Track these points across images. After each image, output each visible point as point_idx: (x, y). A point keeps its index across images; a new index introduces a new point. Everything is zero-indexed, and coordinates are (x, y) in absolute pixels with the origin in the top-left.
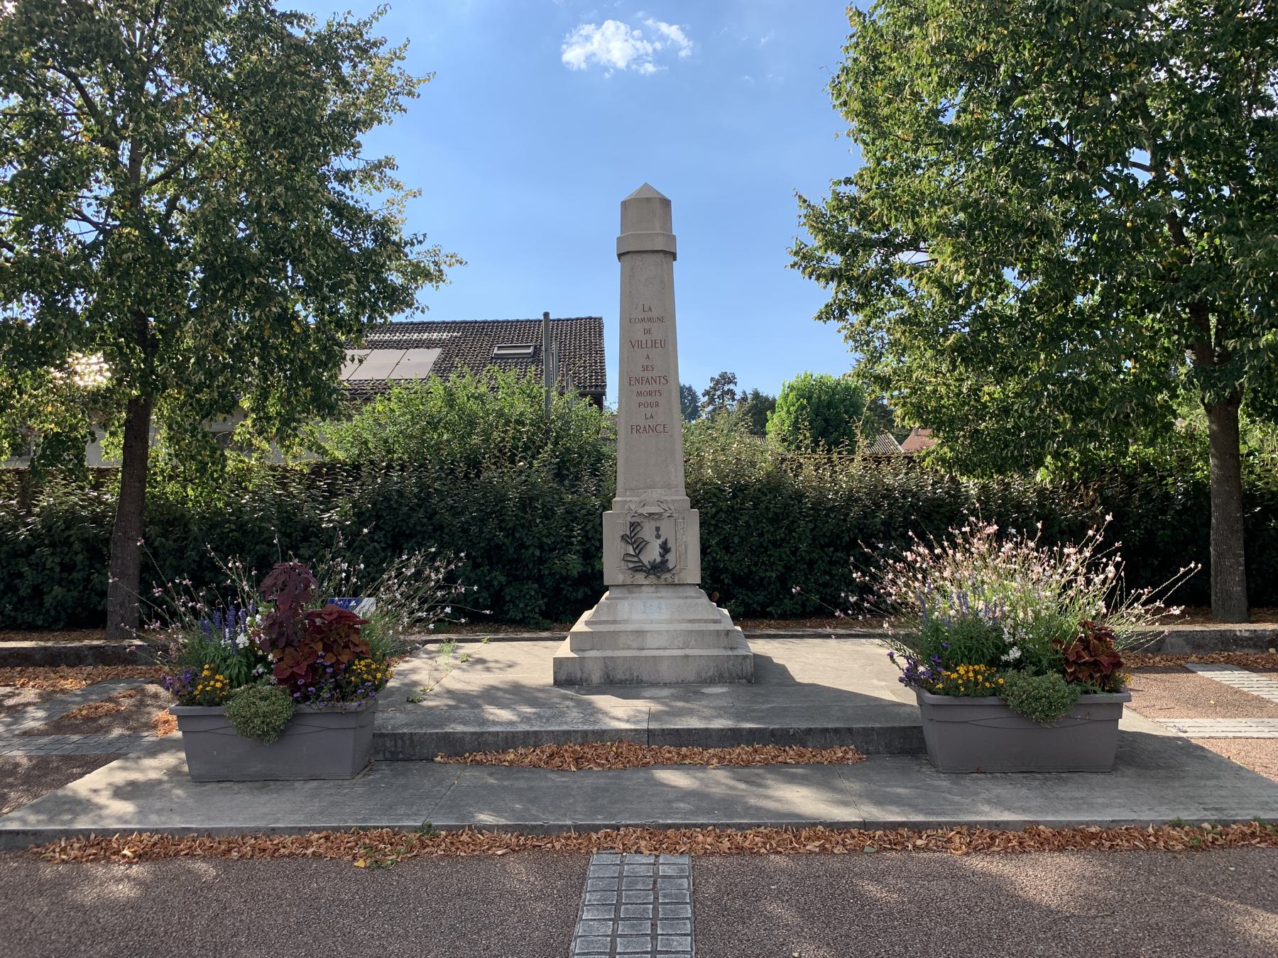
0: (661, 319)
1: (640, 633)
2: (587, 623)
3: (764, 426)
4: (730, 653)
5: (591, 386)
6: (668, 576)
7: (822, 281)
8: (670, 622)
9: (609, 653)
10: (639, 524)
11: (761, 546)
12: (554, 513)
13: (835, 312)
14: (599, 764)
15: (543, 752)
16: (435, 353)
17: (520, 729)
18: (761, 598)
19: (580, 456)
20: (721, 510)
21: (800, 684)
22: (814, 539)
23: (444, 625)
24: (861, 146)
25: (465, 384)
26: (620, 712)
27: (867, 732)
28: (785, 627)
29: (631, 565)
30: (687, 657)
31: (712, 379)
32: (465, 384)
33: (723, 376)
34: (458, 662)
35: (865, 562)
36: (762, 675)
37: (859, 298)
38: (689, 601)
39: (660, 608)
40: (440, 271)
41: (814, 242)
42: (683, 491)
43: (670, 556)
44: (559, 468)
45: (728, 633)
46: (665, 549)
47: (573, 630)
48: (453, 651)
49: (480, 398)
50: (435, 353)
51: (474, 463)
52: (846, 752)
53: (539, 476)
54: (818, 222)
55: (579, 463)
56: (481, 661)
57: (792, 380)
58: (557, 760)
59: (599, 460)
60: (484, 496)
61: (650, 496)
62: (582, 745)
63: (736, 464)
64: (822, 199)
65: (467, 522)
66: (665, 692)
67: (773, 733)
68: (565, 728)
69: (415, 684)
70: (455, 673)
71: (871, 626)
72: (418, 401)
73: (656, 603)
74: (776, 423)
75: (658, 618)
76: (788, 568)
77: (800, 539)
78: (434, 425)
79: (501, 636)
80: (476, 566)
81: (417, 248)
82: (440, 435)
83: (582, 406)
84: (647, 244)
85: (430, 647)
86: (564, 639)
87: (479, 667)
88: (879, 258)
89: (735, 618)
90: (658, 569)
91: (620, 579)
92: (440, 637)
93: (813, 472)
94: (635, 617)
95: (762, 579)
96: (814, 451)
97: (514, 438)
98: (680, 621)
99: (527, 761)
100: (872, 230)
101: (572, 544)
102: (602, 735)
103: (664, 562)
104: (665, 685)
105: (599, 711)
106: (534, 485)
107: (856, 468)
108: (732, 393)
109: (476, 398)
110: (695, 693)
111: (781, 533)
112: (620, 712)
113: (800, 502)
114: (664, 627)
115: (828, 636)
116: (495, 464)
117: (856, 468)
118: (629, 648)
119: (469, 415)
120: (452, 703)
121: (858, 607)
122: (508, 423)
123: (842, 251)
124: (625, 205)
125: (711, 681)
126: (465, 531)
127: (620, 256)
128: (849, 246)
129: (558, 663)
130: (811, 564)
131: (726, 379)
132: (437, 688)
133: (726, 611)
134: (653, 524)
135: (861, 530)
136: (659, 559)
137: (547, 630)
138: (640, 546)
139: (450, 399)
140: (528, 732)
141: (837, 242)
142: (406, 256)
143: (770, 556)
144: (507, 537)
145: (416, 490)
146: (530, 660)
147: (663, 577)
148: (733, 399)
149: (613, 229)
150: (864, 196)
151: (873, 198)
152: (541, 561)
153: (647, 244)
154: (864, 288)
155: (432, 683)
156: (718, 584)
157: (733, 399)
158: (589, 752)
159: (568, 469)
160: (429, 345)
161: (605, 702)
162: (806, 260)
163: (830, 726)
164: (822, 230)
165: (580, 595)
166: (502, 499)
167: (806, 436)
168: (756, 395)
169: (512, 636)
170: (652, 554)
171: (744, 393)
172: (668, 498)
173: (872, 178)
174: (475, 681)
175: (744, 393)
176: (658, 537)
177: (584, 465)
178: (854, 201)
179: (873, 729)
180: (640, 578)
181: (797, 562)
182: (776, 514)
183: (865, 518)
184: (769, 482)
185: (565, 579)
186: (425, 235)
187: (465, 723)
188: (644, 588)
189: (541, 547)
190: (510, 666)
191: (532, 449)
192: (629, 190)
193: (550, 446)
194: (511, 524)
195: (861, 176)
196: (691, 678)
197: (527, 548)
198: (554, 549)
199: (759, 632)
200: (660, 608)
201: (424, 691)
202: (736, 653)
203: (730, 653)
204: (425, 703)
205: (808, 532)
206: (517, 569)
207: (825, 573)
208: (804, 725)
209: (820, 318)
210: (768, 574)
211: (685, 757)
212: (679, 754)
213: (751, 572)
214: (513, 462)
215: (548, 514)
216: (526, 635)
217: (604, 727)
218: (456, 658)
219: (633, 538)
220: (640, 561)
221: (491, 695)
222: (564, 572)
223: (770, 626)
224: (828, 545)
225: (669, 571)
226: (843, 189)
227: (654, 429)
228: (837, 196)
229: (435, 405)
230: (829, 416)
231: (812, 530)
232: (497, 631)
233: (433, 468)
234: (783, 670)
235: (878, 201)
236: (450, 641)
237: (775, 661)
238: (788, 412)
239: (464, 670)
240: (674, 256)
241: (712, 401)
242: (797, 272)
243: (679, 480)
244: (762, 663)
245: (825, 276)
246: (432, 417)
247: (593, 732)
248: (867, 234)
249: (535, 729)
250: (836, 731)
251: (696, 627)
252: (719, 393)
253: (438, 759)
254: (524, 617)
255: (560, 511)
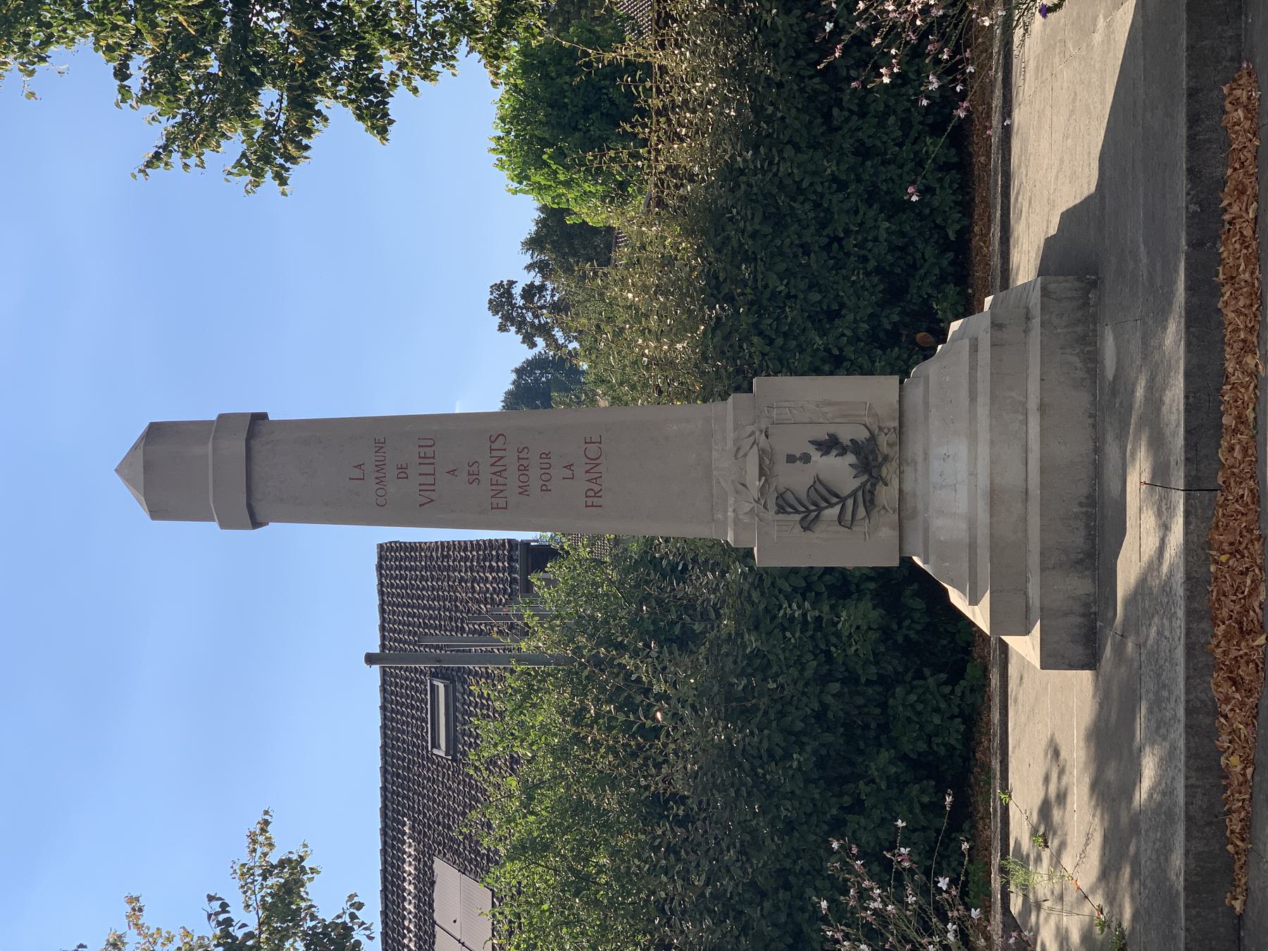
0: (380, 446)
1: (995, 497)
2: (974, 601)
3: (595, 231)
4: (1036, 322)
5: (511, 570)
6: (883, 440)
7: (313, 122)
8: (973, 438)
9: (1034, 560)
10: (781, 496)
11: (827, 248)
12: (757, 653)
13: (373, 110)
14: (1254, 590)
15: (1227, 700)
16: (444, 871)
17: (1181, 743)
18: (929, 252)
19: (645, 599)
20: (756, 325)
21: (1100, 186)
22: (814, 146)
23: (973, 889)
24: (53, 49)
25: (504, 816)
26: (1150, 540)
27: (1196, 58)
28: (988, 206)
29: (861, 512)
30: (1043, 408)
31: (502, 328)
32: (504, 816)
33: (495, 307)
34: (1046, 855)
35: (864, 56)
36: (1080, 254)
37: (348, 54)
38: (932, 400)
39: (946, 457)
40: (282, 864)
41: (234, 144)
42: (715, 407)
43: (846, 435)
44: (670, 640)
45: (996, 325)
46: (829, 445)
47: (987, 630)
48: (1024, 861)
49: (529, 791)
50: (444, 871)
51: (657, 807)
52: (1236, 103)
53: (685, 682)
54: (193, 135)
55: (660, 602)
56: (1045, 810)
57: (504, 179)
58: (1245, 671)
59: (655, 564)
60: (722, 789)
61: (725, 474)
62: (1214, 621)
63: (666, 294)
64: (149, 126)
65: (772, 824)
66: (1112, 450)
67: (1196, 244)
68: (1180, 653)
69: (1087, 937)
70: (1068, 861)
71: (987, 50)
72: (535, 912)
73: (936, 465)
74: (593, 213)
75: (962, 457)
76: (871, 196)
77: (815, 173)
78: (581, 883)
79: (996, 764)
80: (858, 806)
81: (237, 913)
82: (601, 869)
83: (549, 588)
84: (225, 470)
85: (1016, 906)
86: (1004, 646)
87: (1056, 814)
88: (273, 15)
89: (968, 308)
90: (869, 459)
91: (887, 534)
92: (996, 883)
93: (686, 144)
94: (962, 506)
95: (891, 249)
96: (645, 142)
97: (610, 729)
98: (973, 418)
99: (1244, 731)
100: (218, 26)
101: (819, 619)
102: (1195, 582)
103: (856, 447)
104: (1098, 450)
105: (1142, 582)
106: (701, 692)
107: (677, 62)
108: (529, 292)
109: (531, 798)
110: (1114, 393)
111: (803, 209)
112: (1150, 540)
113: (742, 172)
114: (984, 451)
115: (1007, 132)
116: (658, 766)
117: (677, 62)
118: (1024, 520)
119: (563, 814)
120: (1127, 872)
121: (951, 71)
122: (577, 739)
123: (254, 84)
124: (156, 513)
125: (1092, 360)
126: (790, 826)
127: (256, 524)
128: (245, 71)
129: (1050, 660)
130: (863, 152)
131: (502, 300)
132: (1098, 900)
133: (955, 326)
134: (781, 467)
135: (799, 55)
136: (851, 458)
137: (985, 671)
138: (823, 494)
139: (529, 849)
140: (1188, 727)
141: (234, 99)
142: (250, 935)
143: (847, 232)
144: (802, 745)
145: (708, 922)
146: (1046, 713)
147: (885, 449)
148: (542, 288)
149: (201, 537)
150: (150, 44)
151: (154, 25)
152: (851, 679)
153: (225, 470)
154: (331, 45)
155: (1087, 909)
156: (901, 339)
157: (542, 288)
158: (1229, 607)
159: (673, 623)
160: (426, 882)
161: (1128, 570)
162: (273, 155)
163: (1183, 131)
164: (213, 124)
165: (919, 604)
166: (727, 753)
167: (616, 157)
168: (534, 243)
169: (996, 701)
170: (839, 471)
171: (529, 268)
172: (731, 435)
173: (115, 27)
174: (1082, 821)
175: (529, 268)
176: (806, 458)
177: (664, 593)
178: (158, 63)
179: (1190, 48)
180: (887, 495)
181: (859, 180)
182: (766, 218)
183: (775, 45)
184: (704, 232)
185: (886, 633)
186: (211, 898)
187: (1165, 851)
188: (908, 487)
189: (823, 680)
190: (1056, 753)
191: (631, 696)
192: (127, 503)
193: (625, 659)
194: (778, 738)
195: (110, 49)
196: (1082, 399)
197: (825, 707)
198: (828, 653)
199: (996, 261)
200: (946, 457)
201: (1103, 925)
202: (1036, 311)
203: (1036, 322)
204: (1126, 924)
205: (802, 157)
206: (866, 727)
207: (882, 124)
208: (1182, 183)
209: (382, 132)
210: (883, 235)
211: (1241, 419)
212: (1235, 431)
213: (878, 270)
214: (656, 731)
215: (760, 664)
216: (996, 717)
217: (1180, 576)
218: (1039, 859)
219: (808, 508)
220: (854, 494)
221: (1111, 790)
222: (873, 636)
223: (985, 236)
224: (827, 117)
225: (873, 438)
226: (136, 83)
227: (594, 462)
228: (147, 96)
229: (541, 877)
230: (569, 114)
231: (798, 149)
232: (987, 768)
233: (667, 886)
234: (1069, 217)
235: (160, 17)
236: (1003, 871)
237: (1053, 231)
238: (567, 184)
239: (1063, 845)
240: (260, 418)
241: (545, 330)
242: (296, 173)
243: (687, 417)
244: (1056, 256)
245: (303, 120)
246: (564, 886)
247: (1190, 598)
248: (223, 37)
249: (1181, 712)
250: (1193, 120)
251: (984, 386)
252: (529, 316)
253: (1238, 905)
254: (961, 714)
255: (753, 641)
